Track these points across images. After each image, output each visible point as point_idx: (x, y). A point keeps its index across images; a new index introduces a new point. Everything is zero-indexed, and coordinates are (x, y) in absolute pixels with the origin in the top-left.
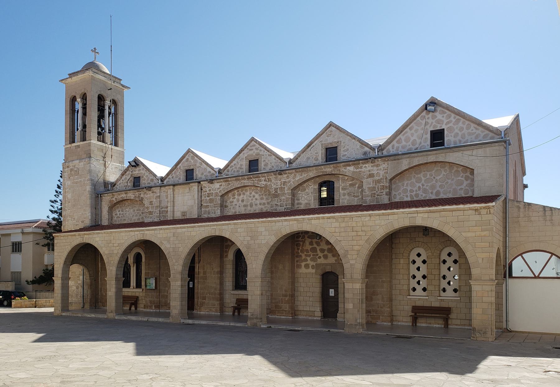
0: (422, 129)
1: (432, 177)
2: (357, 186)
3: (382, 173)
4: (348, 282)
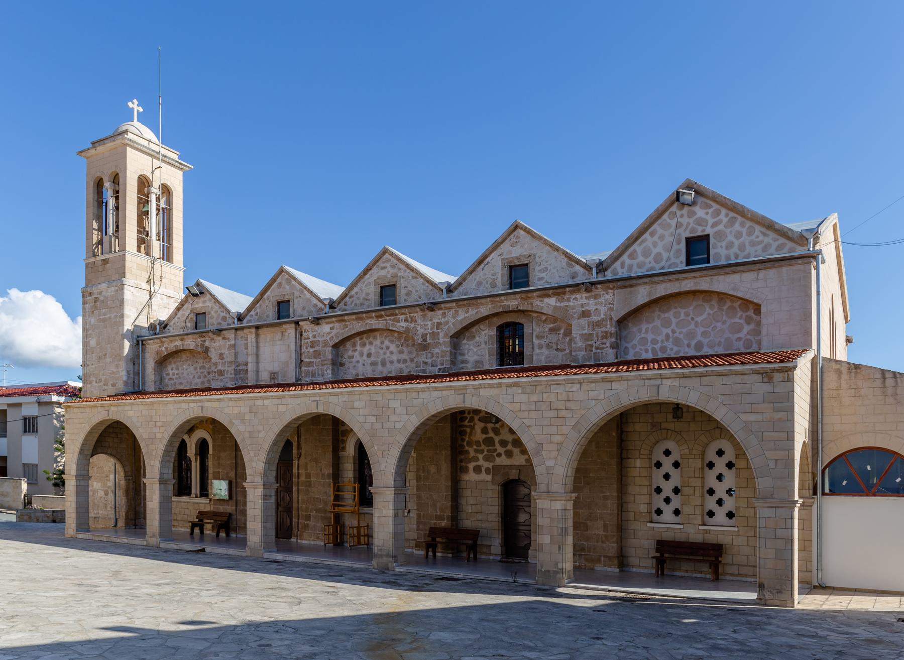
0: (672, 235)
1: (689, 318)
2: (562, 331)
3: (603, 309)
4: (542, 498)
